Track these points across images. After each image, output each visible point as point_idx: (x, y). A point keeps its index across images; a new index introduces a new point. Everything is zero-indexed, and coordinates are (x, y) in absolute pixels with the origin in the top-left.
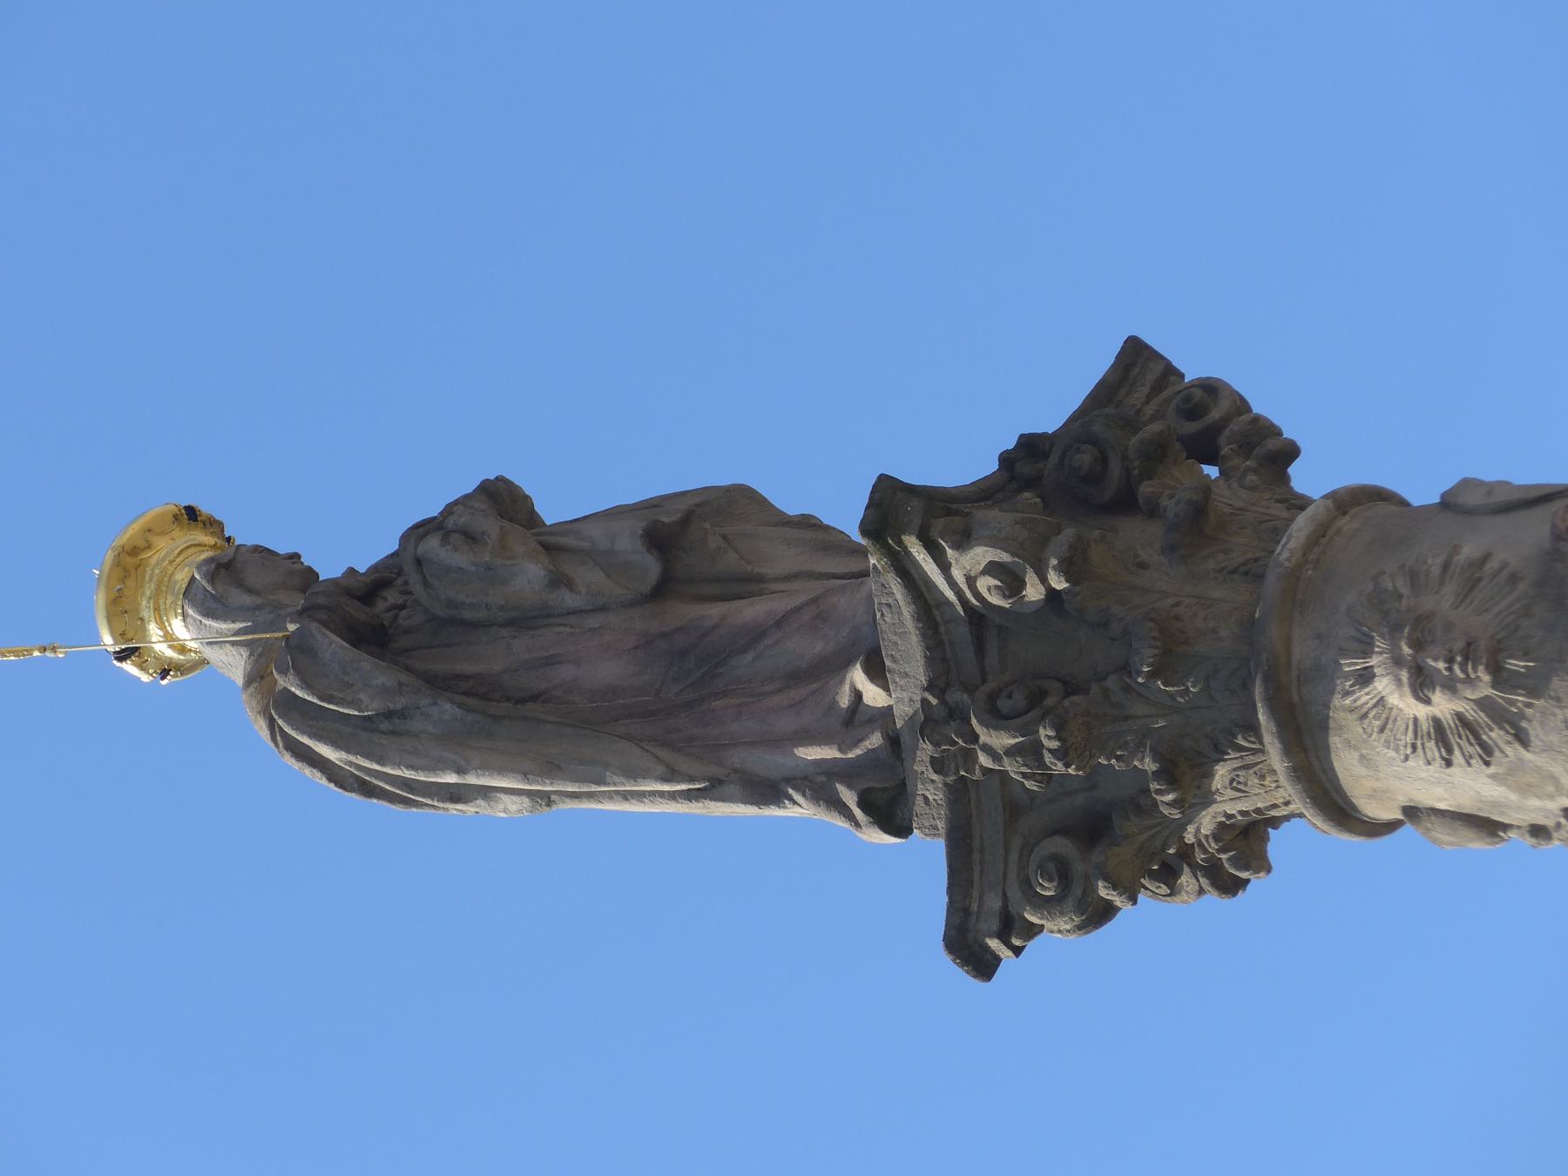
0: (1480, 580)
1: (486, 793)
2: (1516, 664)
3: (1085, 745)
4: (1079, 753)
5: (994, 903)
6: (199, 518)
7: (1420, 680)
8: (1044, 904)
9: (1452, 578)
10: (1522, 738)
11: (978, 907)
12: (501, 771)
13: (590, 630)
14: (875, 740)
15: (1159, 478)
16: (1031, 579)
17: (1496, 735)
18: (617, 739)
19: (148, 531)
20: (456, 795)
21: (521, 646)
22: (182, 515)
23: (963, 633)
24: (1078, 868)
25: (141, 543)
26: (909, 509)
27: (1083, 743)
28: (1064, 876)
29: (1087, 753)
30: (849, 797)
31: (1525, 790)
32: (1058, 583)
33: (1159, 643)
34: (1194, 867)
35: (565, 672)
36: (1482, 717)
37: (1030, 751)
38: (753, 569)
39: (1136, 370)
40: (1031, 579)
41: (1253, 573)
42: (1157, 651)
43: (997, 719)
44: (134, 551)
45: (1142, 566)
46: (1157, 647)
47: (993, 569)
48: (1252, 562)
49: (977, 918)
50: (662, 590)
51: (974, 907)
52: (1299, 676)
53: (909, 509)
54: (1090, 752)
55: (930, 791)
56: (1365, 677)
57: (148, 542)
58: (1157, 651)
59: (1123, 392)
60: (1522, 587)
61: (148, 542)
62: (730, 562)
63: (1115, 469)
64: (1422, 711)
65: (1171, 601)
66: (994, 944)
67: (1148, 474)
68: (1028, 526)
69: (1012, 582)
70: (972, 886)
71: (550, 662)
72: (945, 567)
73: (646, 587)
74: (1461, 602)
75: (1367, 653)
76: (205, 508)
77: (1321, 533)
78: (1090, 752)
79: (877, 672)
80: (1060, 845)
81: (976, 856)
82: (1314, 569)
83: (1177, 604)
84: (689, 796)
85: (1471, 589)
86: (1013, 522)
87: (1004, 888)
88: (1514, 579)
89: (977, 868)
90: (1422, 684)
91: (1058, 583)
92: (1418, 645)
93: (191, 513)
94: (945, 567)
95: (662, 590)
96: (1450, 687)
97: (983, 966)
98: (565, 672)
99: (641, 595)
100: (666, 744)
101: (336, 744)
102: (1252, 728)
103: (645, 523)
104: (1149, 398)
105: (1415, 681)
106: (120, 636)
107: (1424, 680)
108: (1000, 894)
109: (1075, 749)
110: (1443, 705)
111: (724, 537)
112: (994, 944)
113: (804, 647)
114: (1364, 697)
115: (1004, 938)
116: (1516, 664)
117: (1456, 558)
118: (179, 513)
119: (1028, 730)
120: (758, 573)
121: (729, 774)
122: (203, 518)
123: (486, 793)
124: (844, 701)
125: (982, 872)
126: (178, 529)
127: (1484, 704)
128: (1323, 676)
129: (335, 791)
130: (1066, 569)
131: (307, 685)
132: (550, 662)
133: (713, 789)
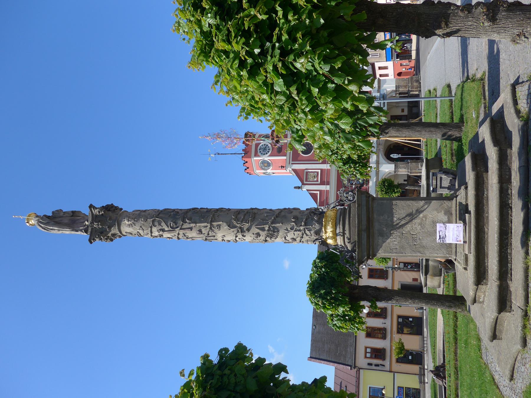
1: (54, 229)
2: (135, 220)
5: (93, 237)
8: (97, 238)
10: (135, 225)
12: (56, 227)
14: (86, 226)
16: (101, 212)
17: (133, 225)
20: (52, 229)
21: (60, 219)
23: (95, 217)
24: (100, 235)
28: (99, 236)
30: (83, 231)
31: (135, 230)
32: (103, 213)
34: (109, 239)
35: (63, 221)
36: (132, 224)
37: (98, 225)
40: (101, 212)
41: (117, 214)
43: (96, 222)
47: (98, 211)
50: (72, 216)
55: (90, 230)
56: (124, 221)
62: (78, 215)
63: (109, 208)
64: (128, 223)
66: (92, 241)
69: (99, 213)
71: (62, 220)
72: (94, 211)
73: (71, 215)
75: (125, 219)
77: (123, 212)
79: (88, 221)
80: (99, 234)
84: (71, 231)
90: (128, 221)
91: (103, 213)
92: (129, 218)
94: (94, 211)
95: (72, 216)
96: (130, 221)
97: (91, 243)
98: (63, 221)
101: (43, 224)
102: (115, 225)
106: (27, 221)
110: (130, 223)
112: (92, 241)
113: (82, 221)
114: (124, 222)
115: (93, 240)
116: (135, 220)
119: (98, 223)
123: (54, 229)
124: (84, 224)
127: (133, 223)
128: (121, 221)
129: (43, 231)
130: (104, 212)
131: (42, 220)
132: (62, 220)
133: (73, 230)
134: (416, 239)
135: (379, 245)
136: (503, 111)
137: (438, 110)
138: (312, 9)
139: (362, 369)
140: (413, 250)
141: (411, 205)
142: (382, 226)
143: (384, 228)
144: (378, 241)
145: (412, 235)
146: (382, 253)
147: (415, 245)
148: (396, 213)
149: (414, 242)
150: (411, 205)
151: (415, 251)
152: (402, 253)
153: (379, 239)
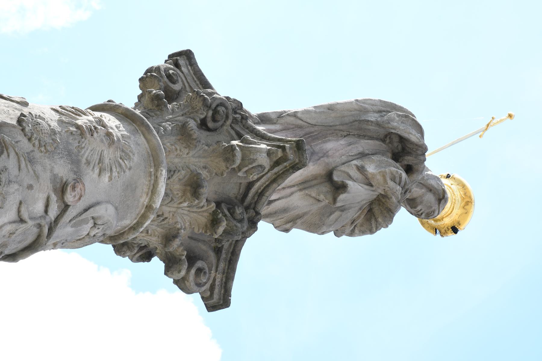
0: (99, 164)
3: (191, 103)
4: (192, 99)
6: (451, 230)
7: (101, 123)
9: (108, 165)
11: (188, 67)
13: (344, 155)
15: (210, 214)
18: (317, 124)
19: (466, 213)
22: (458, 226)
25: (466, 207)
26: (292, 156)
27: (192, 103)
29: (189, 101)
33: (190, 129)
38: (305, 192)
39: (222, 292)
42: (189, 126)
44: (467, 203)
45: (205, 168)
46: (190, 128)
48: (170, 177)
49: (187, 64)
50: (329, 176)
51: (189, 67)
52: (138, 131)
53: (292, 156)
54: (188, 102)
57: (465, 209)
58: (189, 126)
59: (224, 280)
60: (84, 161)
61: (465, 209)
65: (190, 154)
67: (214, 213)
68: (252, 160)
70: (194, 74)
71: (350, 144)
74: (101, 153)
76: (452, 237)
78: (188, 102)
81: (198, 82)
82: (151, 172)
83: (188, 154)
85: (100, 159)
86: (257, 159)
87: (184, 74)
88: (88, 163)
89: (196, 79)
93: (455, 230)
99: (335, 170)
100: (300, 127)
103: (349, 189)
104: (214, 280)
105: (103, 123)
107: (100, 123)
108: (184, 73)
109: (194, 98)
111: (319, 201)
117: (109, 174)
118: (459, 226)
120: (303, 191)
121: (277, 121)
122: (449, 232)
125: (193, 79)
126: (457, 219)
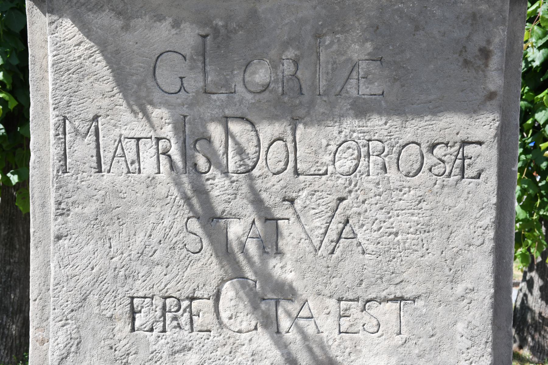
134: (184, 319)
135: (126, 28)
136: (43, 13)
137: (49, 63)
138: (5, 134)
139: (230, 117)
140: (93, 299)
141: (460, 289)
142: (291, 53)
143: (274, 66)
144: (160, 18)
145: (210, 290)
146: (58, 46)
147: (133, 312)
148: (392, 173)
149: (158, 302)
150: (460, 289)
151: (82, 315)
152: (62, 213)
153: (176, 24)
